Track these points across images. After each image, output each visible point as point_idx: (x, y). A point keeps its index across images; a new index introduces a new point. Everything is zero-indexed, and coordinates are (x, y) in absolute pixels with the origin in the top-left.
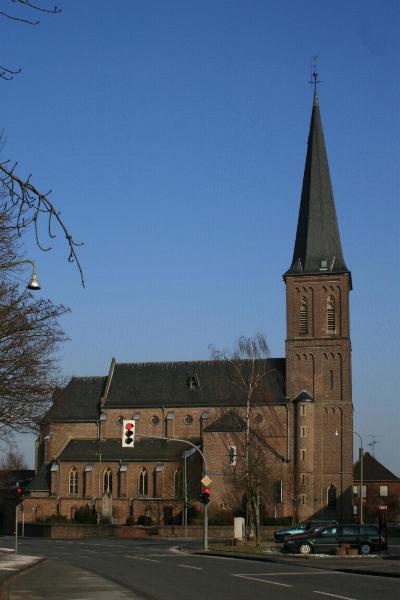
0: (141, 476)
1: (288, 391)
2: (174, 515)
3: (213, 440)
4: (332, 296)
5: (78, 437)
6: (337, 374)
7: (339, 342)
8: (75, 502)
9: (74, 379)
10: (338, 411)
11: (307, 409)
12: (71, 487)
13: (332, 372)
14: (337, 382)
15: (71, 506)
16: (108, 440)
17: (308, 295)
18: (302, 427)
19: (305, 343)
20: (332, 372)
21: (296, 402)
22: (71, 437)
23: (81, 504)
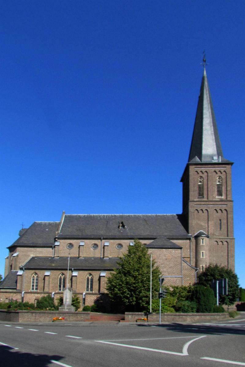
0: (88, 279)
1: (190, 231)
2: (188, 355)
3: (235, 287)
4: (220, 176)
5: (38, 255)
6: (224, 222)
7: (226, 203)
8: (36, 295)
9: (237, 275)
10: (225, 243)
11: (204, 242)
12: (33, 286)
13: (220, 220)
14: (224, 227)
15: (34, 298)
16: (61, 258)
17: (223, 176)
18: (201, 252)
19: (203, 203)
20: (220, 220)
21: (197, 237)
22: (32, 256)
23: (40, 296)
